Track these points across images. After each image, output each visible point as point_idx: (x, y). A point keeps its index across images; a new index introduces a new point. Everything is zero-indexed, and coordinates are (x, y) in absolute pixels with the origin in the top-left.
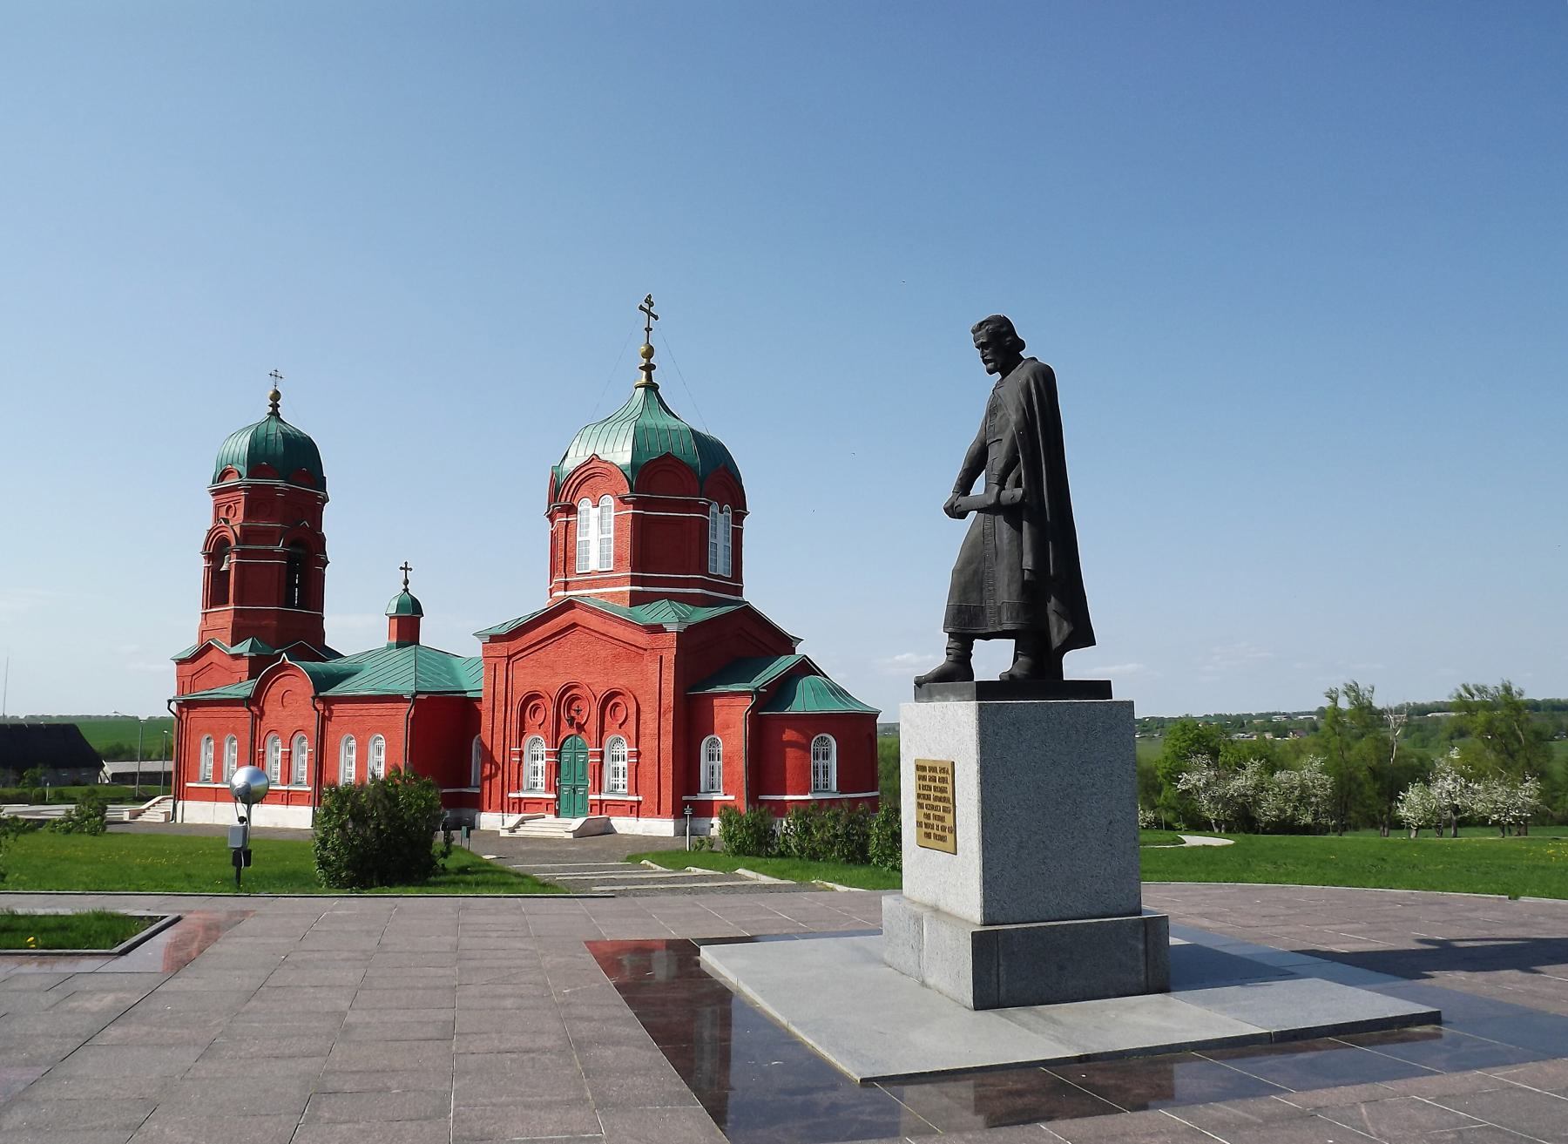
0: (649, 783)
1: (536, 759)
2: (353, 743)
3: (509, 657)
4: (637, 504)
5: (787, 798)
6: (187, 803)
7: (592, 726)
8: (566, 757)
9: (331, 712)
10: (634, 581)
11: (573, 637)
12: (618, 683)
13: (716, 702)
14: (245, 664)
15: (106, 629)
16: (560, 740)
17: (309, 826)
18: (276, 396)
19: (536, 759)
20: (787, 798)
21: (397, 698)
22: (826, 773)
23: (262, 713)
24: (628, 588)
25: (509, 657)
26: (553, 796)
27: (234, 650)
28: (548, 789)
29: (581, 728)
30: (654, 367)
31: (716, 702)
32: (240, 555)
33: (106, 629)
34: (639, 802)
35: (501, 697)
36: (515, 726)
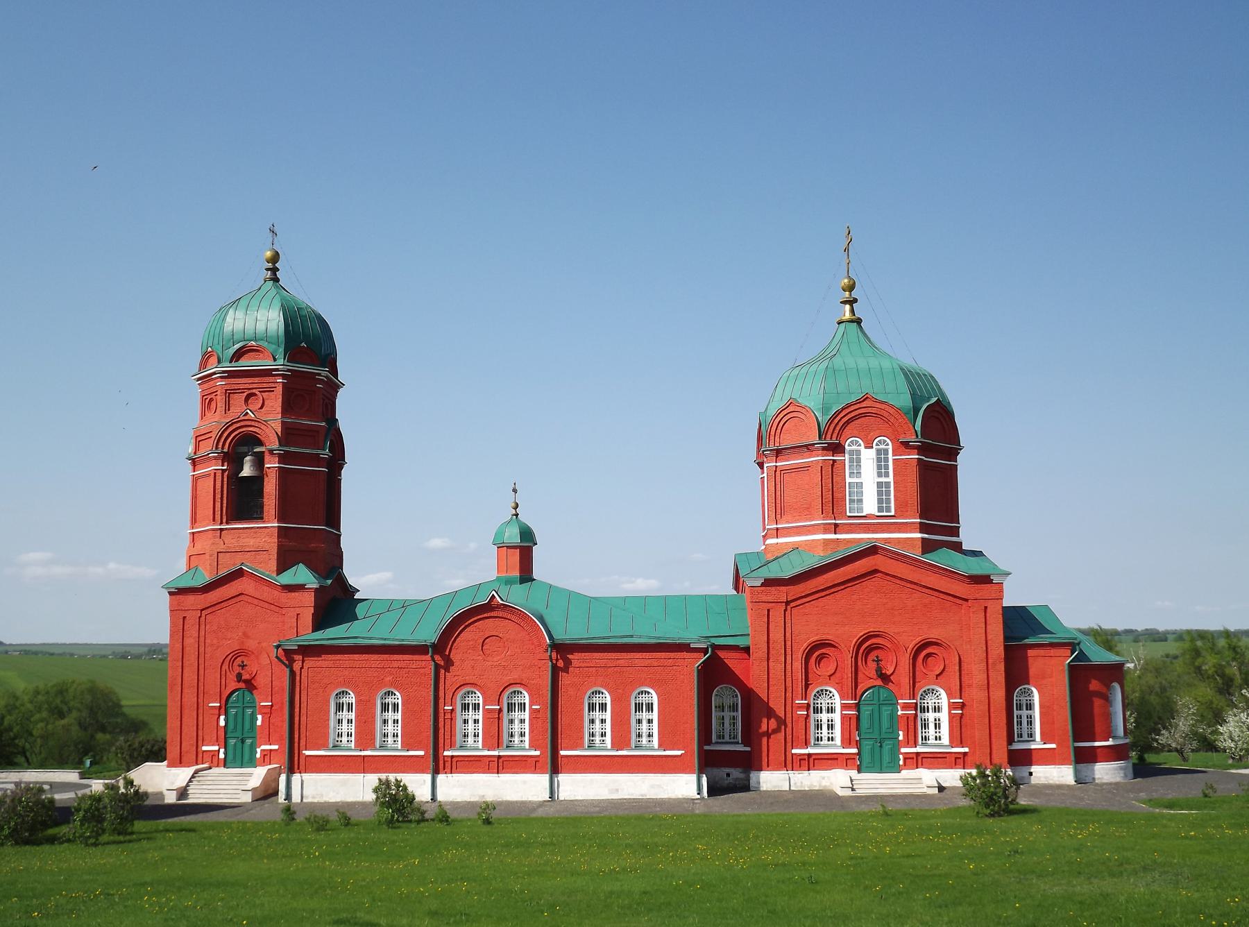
0: (980, 733)
1: (832, 709)
2: (351, 698)
3: (787, 603)
4: (922, 449)
5: (1097, 744)
6: (306, 776)
7: (903, 677)
8: (866, 711)
9: (568, 663)
10: (923, 528)
11: (876, 581)
12: (933, 634)
13: (1030, 653)
14: (309, 599)
15: (89, 550)
16: (859, 693)
17: (561, 798)
18: (275, 258)
19: (832, 709)
20: (1097, 744)
21: (683, 647)
22: (1030, 723)
23: (449, 663)
24: (919, 535)
25: (787, 603)
26: (855, 751)
27: (287, 578)
28: (847, 742)
29: (885, 678)
30: (855, 300)
31: (1030, 653)
32: (283, 458)
33: (89, 550)
34: (965, 754)
35: (778, 647)
36: (799, 676)
